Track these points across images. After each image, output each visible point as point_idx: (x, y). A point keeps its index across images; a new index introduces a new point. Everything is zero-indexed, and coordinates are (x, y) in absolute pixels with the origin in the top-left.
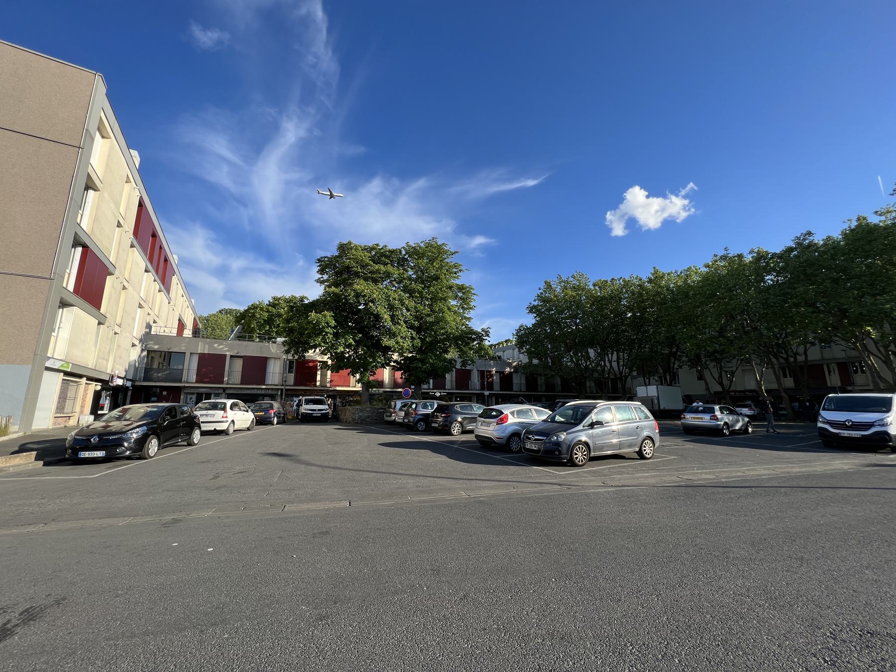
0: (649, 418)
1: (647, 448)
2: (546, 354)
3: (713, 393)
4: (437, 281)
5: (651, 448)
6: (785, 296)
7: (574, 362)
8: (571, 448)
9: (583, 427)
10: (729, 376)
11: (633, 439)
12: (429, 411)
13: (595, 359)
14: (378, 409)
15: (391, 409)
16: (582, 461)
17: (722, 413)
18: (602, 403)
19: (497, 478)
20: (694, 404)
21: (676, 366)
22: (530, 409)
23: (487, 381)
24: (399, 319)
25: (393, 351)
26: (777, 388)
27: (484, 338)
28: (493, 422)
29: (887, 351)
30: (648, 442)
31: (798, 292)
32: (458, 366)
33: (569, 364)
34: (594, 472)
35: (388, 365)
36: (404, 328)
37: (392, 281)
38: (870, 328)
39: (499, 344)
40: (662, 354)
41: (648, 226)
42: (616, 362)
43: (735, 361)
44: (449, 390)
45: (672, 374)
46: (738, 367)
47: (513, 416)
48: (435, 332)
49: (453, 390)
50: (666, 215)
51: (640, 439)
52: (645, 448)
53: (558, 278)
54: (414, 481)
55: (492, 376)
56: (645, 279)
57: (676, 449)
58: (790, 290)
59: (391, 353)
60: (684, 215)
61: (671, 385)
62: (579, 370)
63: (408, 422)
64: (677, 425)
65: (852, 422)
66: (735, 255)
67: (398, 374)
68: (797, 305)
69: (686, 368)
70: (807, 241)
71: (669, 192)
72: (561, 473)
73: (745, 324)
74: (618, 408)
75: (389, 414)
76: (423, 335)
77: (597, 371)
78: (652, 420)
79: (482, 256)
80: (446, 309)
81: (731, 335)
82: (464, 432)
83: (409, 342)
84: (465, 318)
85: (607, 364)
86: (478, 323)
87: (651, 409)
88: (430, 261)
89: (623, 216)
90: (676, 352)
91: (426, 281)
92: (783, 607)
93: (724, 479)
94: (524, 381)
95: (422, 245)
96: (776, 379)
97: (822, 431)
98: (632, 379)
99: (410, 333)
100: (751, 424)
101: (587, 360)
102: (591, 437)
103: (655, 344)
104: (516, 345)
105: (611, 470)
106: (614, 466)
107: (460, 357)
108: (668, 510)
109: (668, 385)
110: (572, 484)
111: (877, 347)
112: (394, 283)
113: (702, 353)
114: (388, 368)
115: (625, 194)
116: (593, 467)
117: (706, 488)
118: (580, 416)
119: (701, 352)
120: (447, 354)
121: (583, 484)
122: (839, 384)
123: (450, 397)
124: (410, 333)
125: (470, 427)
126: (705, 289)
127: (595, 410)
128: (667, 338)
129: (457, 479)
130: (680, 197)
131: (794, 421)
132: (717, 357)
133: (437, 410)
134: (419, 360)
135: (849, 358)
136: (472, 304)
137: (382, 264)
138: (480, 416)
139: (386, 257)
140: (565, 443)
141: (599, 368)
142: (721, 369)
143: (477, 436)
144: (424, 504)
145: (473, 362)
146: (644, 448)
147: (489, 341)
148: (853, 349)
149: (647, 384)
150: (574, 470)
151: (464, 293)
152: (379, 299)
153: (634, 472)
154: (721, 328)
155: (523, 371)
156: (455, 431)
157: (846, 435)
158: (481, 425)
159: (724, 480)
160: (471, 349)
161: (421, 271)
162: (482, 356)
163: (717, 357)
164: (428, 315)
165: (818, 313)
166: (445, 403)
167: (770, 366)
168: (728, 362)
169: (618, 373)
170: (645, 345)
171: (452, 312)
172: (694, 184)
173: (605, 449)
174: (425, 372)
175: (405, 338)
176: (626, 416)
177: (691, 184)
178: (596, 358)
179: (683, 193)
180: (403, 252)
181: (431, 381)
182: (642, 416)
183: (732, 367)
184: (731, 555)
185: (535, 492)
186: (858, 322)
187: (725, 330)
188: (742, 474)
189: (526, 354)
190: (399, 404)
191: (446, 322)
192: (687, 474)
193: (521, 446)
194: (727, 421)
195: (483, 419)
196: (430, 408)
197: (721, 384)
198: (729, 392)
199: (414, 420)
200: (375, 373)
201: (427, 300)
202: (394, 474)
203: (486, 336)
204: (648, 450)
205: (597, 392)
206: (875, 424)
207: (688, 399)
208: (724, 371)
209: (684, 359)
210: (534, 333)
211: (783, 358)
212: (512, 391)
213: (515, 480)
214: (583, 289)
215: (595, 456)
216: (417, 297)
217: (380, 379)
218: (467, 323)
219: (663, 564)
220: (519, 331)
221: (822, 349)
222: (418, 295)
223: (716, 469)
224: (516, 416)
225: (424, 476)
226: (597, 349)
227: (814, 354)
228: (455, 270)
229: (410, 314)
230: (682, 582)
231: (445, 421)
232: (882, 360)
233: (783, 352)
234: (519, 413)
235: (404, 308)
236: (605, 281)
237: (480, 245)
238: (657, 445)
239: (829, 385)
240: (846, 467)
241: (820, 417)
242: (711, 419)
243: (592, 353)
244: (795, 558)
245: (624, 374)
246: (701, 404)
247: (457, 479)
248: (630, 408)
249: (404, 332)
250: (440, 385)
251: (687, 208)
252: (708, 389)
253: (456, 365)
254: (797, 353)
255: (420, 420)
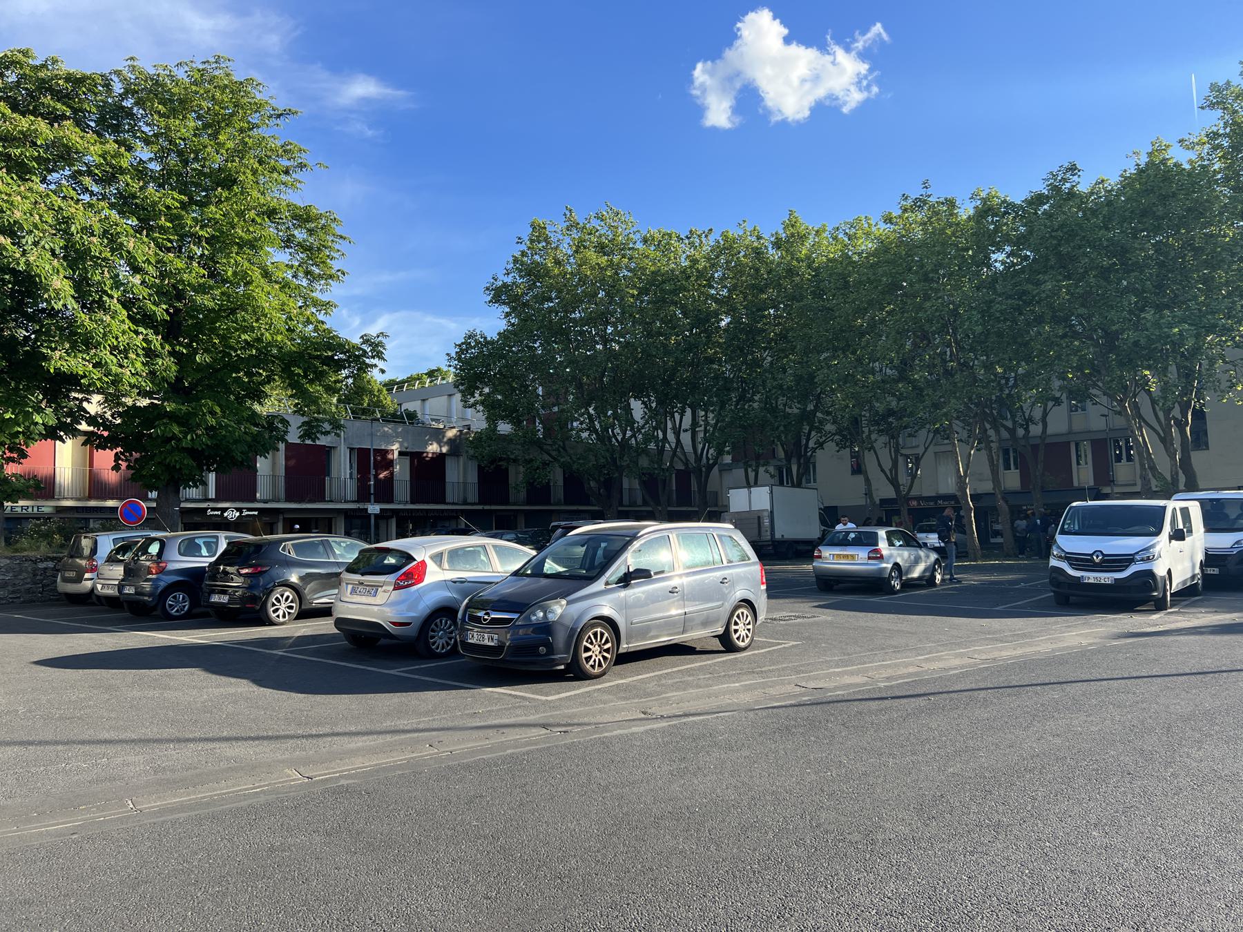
0: (749, 559)
1: (741, 627)
2: (530, 408)
3: (878, 502)
4: (229, 189)
5: (749, 627)
6: (1020, 298)
7: (596, 431)
8: (576, 636)
9: (607, 583)
10: (910, 466)
11: (713, 608)
12: (204, 560)
13: (645, 424)
14: (35, 562)
15: (81, 557)
16: (600, 665)
17: (891, 544)
18: (651, 528)
19: (387, 724)
20: (839, 527)
21: (811, 444)
22: (484, 547)
23: (376, 476)
24: (105, 292)
25: (87, 390)
26: (993, 492)
27: (367, 361)
28: (385, 583)
29: (1168, 419)
30: (743, 613)
31: (1044, 291)
32: (293, 437)
33: (585, 435)
34: (626, 688)
35: (74, 432)
36: (123, 322)
37: (80, 172)
38: (1148, 373)
39: (410, 380)
40: (787, 416)
41: (783, 114)
42: (689, 433)
43: (923, 433)
44: (266, 502)
45: (802, 461)
46: (928, 446)
47: (440, 566)
48: (224, 338)
49: (278, 501)
50: (821, 92)
51: (728, 606)
52: (736, 627)
53: (565, 215)
54: (147, 757)
55: (389, 464)
56: (768, 238)
57: (799, 624)
58: (1030, 287)
59: (80, 396)
60: (856, 97)
61: (799, 485)
62: (608, 451)
63: (137, 593)
64: (806, 574)
65: (1104, 555)
66: (941, 200)
67: (105, 459)
68: (1040, 320)
69: (830, 446)
70: (1068, 185)
71: (831, 39)
72: (550, 698)
73: (948, 353)
74: (686, 538)
75: (72, 574)
76: (189, 346)
77: (646, 452)
78: (754, 564)
79: (370, 133)
80: (256, 274)
81: (921, 377)
82: (306, 614)
83: (138, 365)
84: (315, 303)
85: (671, 436)
86: (357, 322)
87: (756, 538)
88: (206, 126)
89: (730, 79)
90: (814, 412)
91: (197, 185)
92: (958, 923)
93: (882, 682)
94: (473, 477)
95: (181, 74)
96: (992, 473)
97: (1054, 575)
98: (720, 471)
99: (141, 337)
100: (940, 566)
101: (627, 426)
102: (623, 606)
103: (773, 392)
104: (456, 386)
105: (663, 682)
106: (670, 670)
107: (299, 411)
108: (772, 756)
109: (793, 486)
110: (576, 721)
111: (1154, 409)
112: (87, 180)
113: (864, 416)
114: (69, 442)
115: (739, 25)
116: (626, 678)
117: (848, 703)
118: (603, 560)
119: (863, 413)
120: (260, 403)
121: (599, 719)
122: (1092, 483)
123: (269, 519)
124: (141, 337)
125: (321, 600)
126: (880, 271)
127: (635, 543)
128: (799, 379)
129: (277, 738)
130: (853, 53)
131: (1016, 557)
132: (890, 424)
133: (226, 558)
134: (172, 417)
135: (1110, 430)
136: (336, 265)
137: (42, 115)
138: (351, 569)
139: (60, 96)
140: (562, 625)
141: (652, 446)
142: (897, 451)
143: (340, 622)
144: (177, 816)
145: (336, 425)
146: (734, 627)
147: (383, 371)
148: (1119, 413)
149: (752, 483)
150: (579, 688)
151: (311, 232)
152: (36, 226)
153: (710, 682)
154: (904, 362)
155: (471, 452)
156: (280, 612)
157: (1091, 581)
158: (353, 592)
159: (882, 685)
160: (331, 390)
161: (180, 153)
162: (364, 411)
163: (890, 424)
164: (202, 289)
165: (1072, 337)
166: (251, 537)
167: (983, 445)
168: (910, 435)
169: (692, 459)
170: (754, 394)
171: (276, 282)
172: (885, 28)
173: (652, 634)
174: (192, 452)
175: (125, 352)
176: (700, 555)
177: (878, 28)
178: (647, 422)
179: (859, 45)
180: (118, 88)
181: (212, 477)
182: (735, 555)
183: (918, 446)
184: (880, 837)
185: (484, 751)
186: (1130, 361)
187: (911, 366)
188: (916, 669)
189: (481, 408)
190: (106, 543)
191: (259, 314)
192: (816, 678)
193: (456, 641)
194: (899, 560)
195: (358, 577)
196: (204, 552)
197: (894, 482)
198: (908, 499)
199: (155, 587)
200: (23, 455)
201: (198, 244)
202: (83, 742)
203: (373, 357)
204: (741, 631)
205: (645, 503)
206: (1137, 557)
207: (830, 516)
208: (902, 455)
209: (829, 427)
210: (504, 357)
211: (1006, 428)
212: (444, 502)
213: (435, 725)
214: (623, 248)
215: (630, 650)
216: (162, 229)
217: (43, 470)
218: (321, 317)
219: (751, 875)
220: (464, 348)
221: (1072, 411)
222: (169, 224)
223: (870, 662)
224: (446, 566)
225: (179, 740)
226: (650, 400)
227: (1059, 422)
228: (284, 163)
229: (143, 282)
230: (786, 908)
231: (250, 588)
232: (1158, 434)
233: (1009, 416)
234: (456, 556)
235: (122, 262)
236: (668, 234)
237: (365, 100)
238: (761, 617)
239: (1076, 484)
240: (1084, 642)
241: (1054, 548)
242: (869, 558)
243: (637, 408)
244: (988, 826)
245: (704, 460)
246: (851, 525)
247: (277, 738)
248: (710, 537)
249: (124, 332)
250: (239, 487)
251: (865, 83)
252: (869, 494)
253: (286, 432)
254: (1030, 420)
255: (172, 588)
